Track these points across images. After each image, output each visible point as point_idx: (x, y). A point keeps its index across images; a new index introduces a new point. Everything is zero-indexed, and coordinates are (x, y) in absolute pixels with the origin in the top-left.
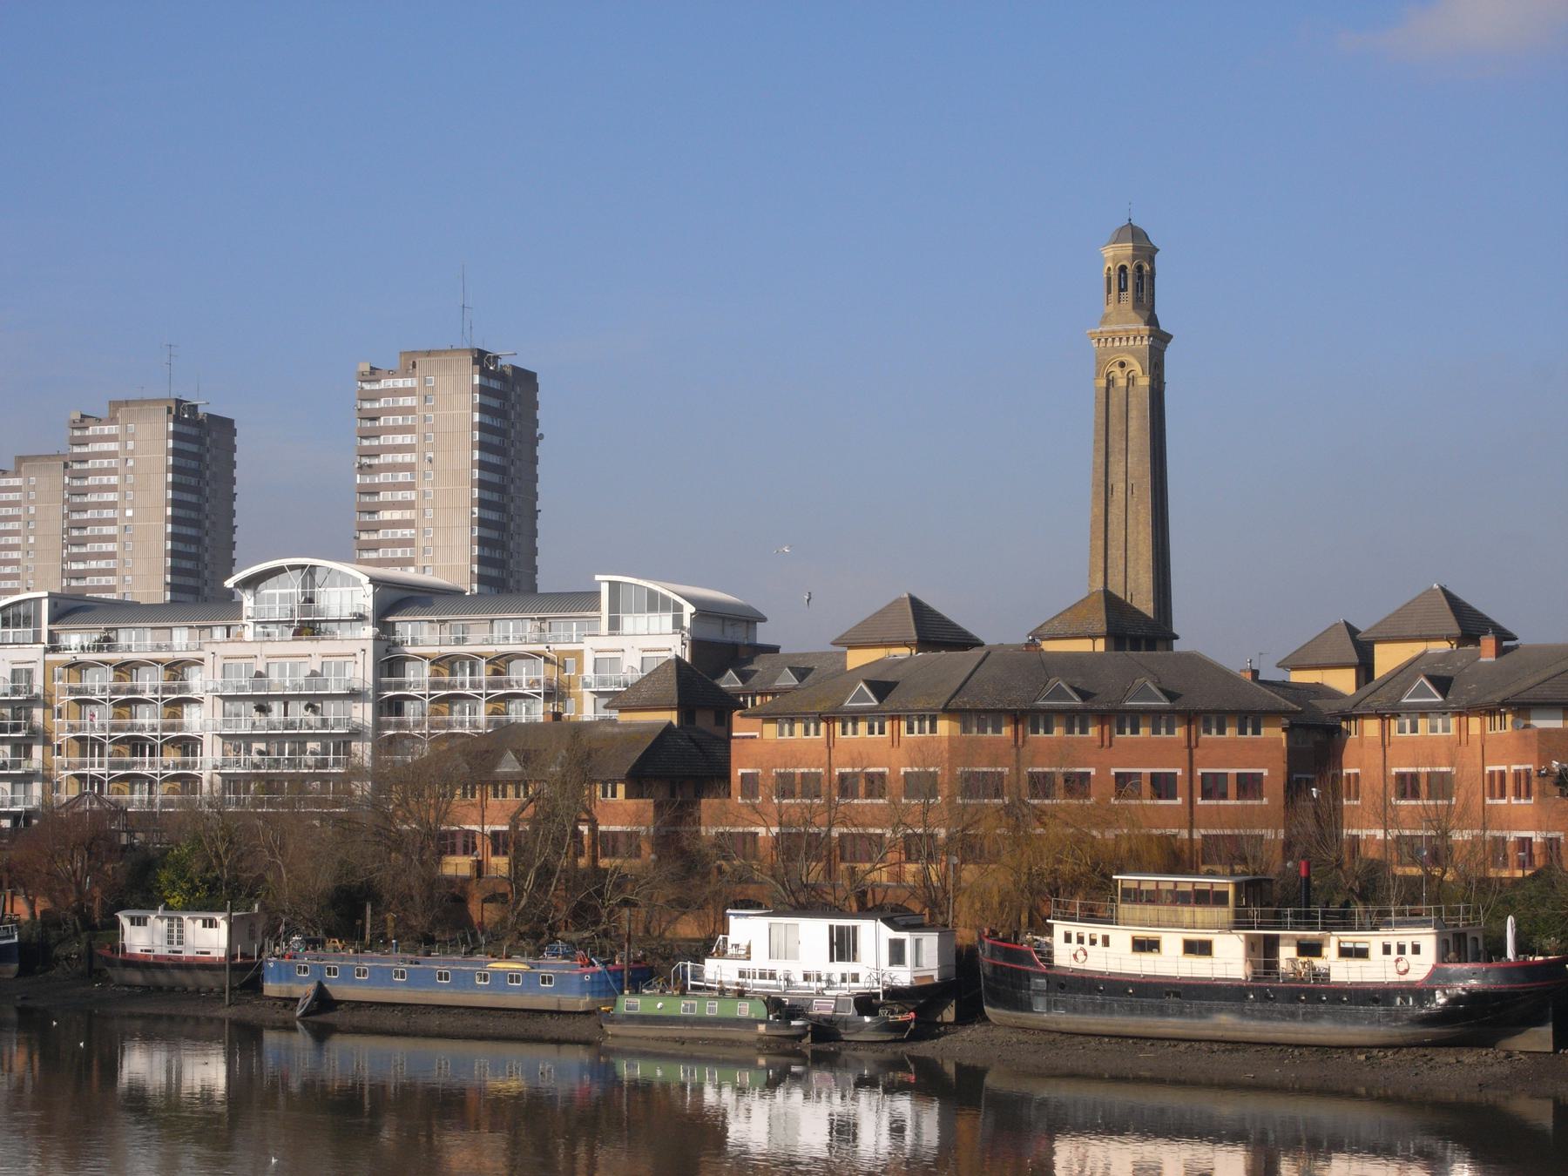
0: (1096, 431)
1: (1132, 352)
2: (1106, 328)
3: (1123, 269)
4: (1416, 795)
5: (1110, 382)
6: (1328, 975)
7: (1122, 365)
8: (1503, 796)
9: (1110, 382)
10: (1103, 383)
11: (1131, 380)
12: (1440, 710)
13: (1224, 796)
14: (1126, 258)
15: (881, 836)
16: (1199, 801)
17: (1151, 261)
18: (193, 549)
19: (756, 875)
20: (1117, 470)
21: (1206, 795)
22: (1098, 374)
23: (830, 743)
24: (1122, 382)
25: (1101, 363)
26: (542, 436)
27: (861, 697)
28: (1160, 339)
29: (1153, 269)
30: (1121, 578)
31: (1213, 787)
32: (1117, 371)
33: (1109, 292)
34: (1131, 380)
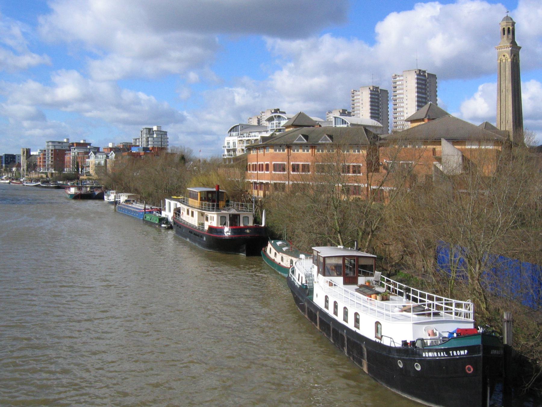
1: (506, 52)
4: (298, 171)
7: (504, 56)
8: (262, 170)
10: (499, 61)
11: (506, 60)
12: (332, 146)
15: (309, 184)
16: (292, 173)
18: (377, 97)
20: (503, 86)
21: (294, 171)
23: (289, 155)
24: (504, 61)
25: (498, 56)
27: (300, 139)
28: (515, 50)
31: (295, 168)
32: (503, 57)
34: (506, 60)
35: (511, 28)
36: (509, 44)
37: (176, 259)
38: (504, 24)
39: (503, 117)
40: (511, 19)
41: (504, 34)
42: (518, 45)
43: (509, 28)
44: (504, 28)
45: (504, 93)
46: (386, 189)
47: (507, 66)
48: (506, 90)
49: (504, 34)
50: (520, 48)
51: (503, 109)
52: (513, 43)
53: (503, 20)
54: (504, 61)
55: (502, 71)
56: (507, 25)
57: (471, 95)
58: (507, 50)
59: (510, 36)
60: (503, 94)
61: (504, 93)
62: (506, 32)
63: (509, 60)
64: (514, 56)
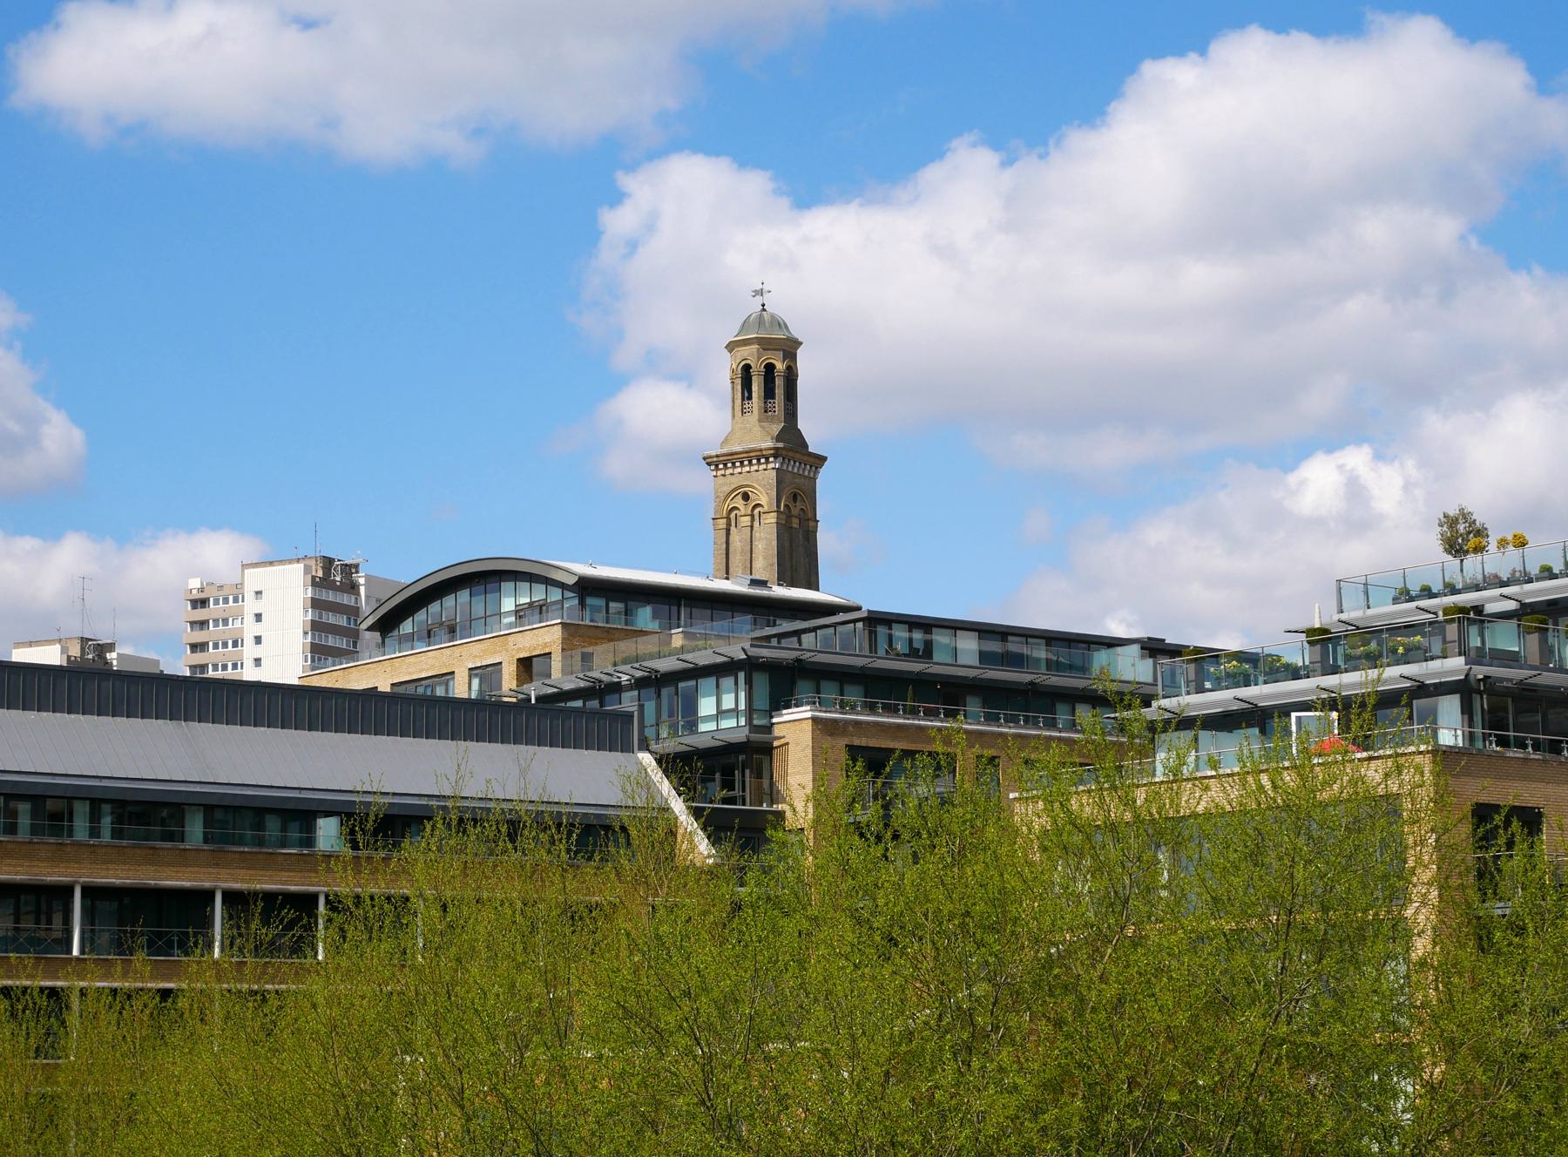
3: (747, 368)
7: (746, 497)
28: (796, 462)
32: (739, 503)
35: (780, 366)
43: (770, 368)
44: (747, 368)
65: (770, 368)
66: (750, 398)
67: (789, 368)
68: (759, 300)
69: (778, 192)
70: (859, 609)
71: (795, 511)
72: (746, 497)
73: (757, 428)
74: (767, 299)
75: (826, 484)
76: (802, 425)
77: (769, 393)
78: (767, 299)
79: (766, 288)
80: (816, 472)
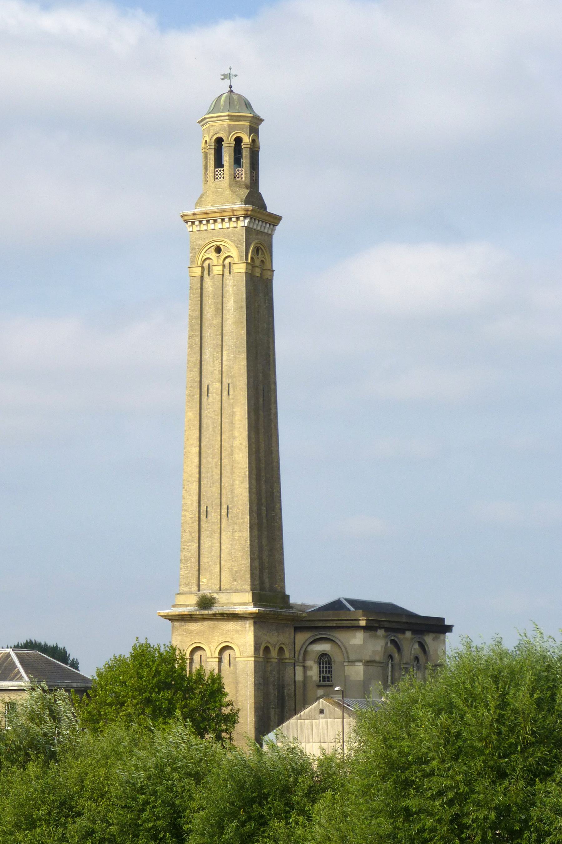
0: (191, 326)
2: (202, 209)
3: (219, 141)
5: (206, 269)
6: (57, 646)
7: (218, 250)
9: (206, 269)
10: (197, 271)
13: (67, 664)
14: (224, 130)
17: (254, 130)
19: (316, 805)
22: (192, 262)
24: (217, 270)
25: (195, 251)
26: (64, 648)
28: (261, 224)
29: (254, 142)
30: (215, 489)
32: (213, 255)
33: (206, 169)
34: (228, 267)
35: (247, 140)
36: (238, 206)
37: (111, 803)
38: (220, 126)
39: (211, 491)
40: (248, 105)
41: (219, 163)
42: (270, 209)
43: (238, 141)
44: (219, 141)
45: (214, 396)
46: (55, 741)
47: (230, 290)
48: (226, 389)
49: (219, 163)
50: (275, 220)
51: (211, 461)
52: (254, 198)
53: (216, 107)
54: (217, 270)
55: (209, 311)
56: (231, 129)
57: (355, 637)
58: (232, 236)
59: (244, 173)
60: (212, 401)
61: (214, 396)
62: (227, 157)
63: (240, 268)
64: (257, 250)
65: (238, 141)
66: (222, 166)
67: (254, 141)
68: (227, 82)
69: (526, 648)
70: (75, 665)
71: (257, 262)
72: (218, 250)
73: (228, 192)
74: (234, 82)
75: (280, 237)
76: (263, 189)
77: (237, 161)
78: (234, 82)
79: (233, 72)
80: (273, 230)
